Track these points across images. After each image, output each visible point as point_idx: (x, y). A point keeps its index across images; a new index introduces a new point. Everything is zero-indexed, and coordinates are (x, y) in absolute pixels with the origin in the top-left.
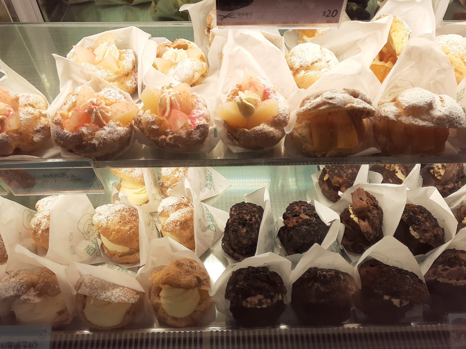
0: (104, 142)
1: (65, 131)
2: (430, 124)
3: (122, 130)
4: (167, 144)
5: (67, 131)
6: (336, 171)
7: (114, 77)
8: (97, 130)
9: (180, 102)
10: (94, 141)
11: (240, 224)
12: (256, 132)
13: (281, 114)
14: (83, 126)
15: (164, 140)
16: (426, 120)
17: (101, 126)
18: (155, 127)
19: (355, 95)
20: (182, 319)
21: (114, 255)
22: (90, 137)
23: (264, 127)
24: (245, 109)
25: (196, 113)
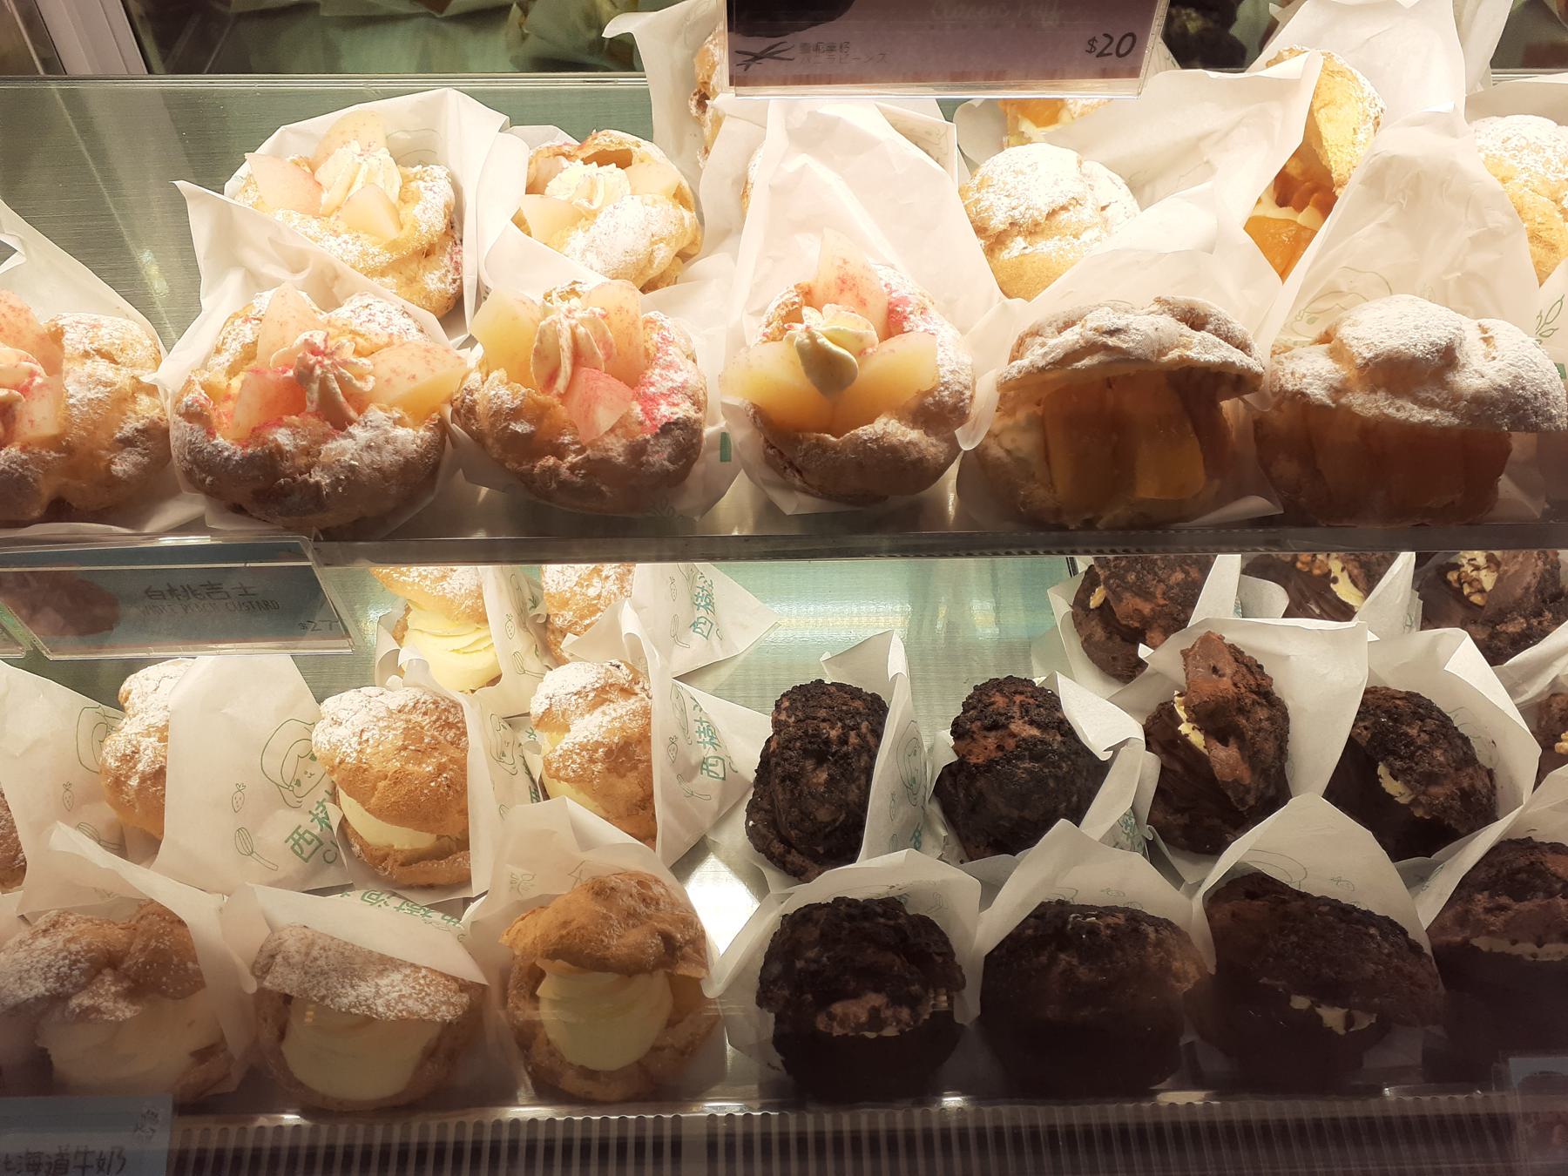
0: (351, 480)
1: (220, 440)
2: (1448, 419)
3: (411, 437)
4: (563, 485)
5: (225, 442)
6: (1132, 577)
7: (385, 258)
8: (326, 437)
9: (606, 345)
10: (317, 476)
11: (806, 753)
12: (861, 446)
13: (946, 385)
14: (279, 423)
15: (553, 472)
16: (1432, 405)
17: (341, 424)
18: (520, 428)
19: (1195, 320)
20: (611, 1075)
21: (385, 858)
22: (302, 461)
23: (890, 428)
24: (825, 367)
25: (659, 380)
